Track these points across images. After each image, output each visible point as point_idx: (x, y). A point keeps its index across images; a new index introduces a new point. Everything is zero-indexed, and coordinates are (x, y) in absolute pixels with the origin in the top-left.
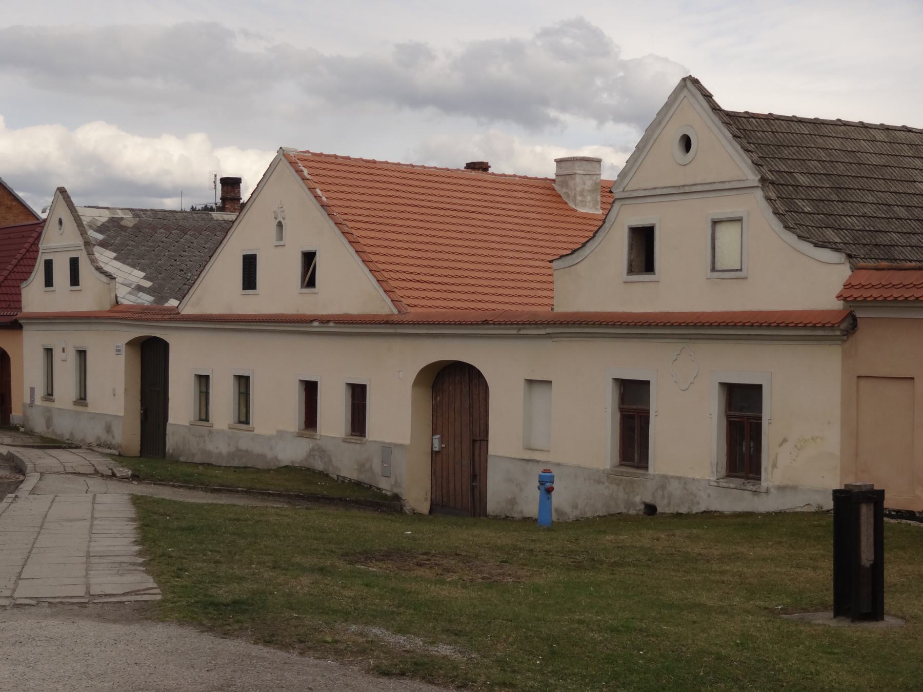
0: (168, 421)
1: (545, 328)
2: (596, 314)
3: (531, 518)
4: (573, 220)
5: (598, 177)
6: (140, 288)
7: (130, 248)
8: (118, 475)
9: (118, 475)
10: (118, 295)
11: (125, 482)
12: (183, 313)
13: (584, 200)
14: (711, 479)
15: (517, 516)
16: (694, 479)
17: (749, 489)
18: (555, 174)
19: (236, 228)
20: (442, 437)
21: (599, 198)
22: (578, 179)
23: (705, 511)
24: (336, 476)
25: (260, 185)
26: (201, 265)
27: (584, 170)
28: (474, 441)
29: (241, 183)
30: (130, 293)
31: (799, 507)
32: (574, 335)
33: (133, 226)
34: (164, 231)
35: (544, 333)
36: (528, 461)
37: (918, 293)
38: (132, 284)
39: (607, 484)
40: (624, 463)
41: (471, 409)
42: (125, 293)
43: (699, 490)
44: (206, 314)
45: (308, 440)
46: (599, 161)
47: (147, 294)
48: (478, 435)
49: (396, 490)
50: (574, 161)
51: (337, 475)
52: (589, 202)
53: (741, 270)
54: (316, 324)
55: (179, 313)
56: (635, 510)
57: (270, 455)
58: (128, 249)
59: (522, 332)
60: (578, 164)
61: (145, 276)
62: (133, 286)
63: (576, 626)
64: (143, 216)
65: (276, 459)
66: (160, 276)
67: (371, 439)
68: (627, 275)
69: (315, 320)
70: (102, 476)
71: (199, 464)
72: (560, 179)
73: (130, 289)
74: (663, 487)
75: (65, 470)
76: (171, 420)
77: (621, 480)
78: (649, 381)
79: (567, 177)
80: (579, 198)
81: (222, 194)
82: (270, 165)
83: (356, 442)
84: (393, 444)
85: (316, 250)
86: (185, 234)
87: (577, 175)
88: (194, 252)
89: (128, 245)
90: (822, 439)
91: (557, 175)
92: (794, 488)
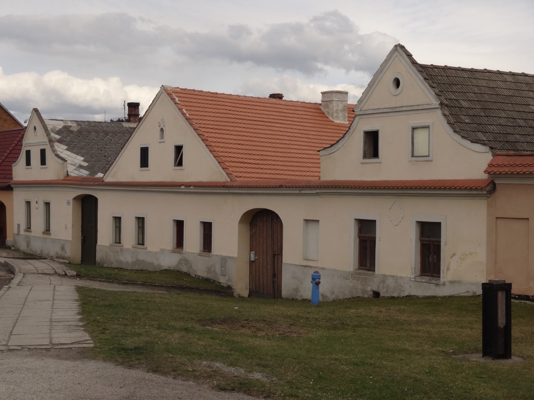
0: (97, 243)
1: (315, 190)
2: (345, 182)
3: (307, 299)
4: (332, 127)
5: (346, 102)
6: (81, 167)
7: (75, 143)
8: (68, 275)
9: (68, 275)
10: (68, 171)
11: (72, 279)
12: (106, 181)
13: (338, 115)
14: (412, 277)
15: (299, 298)
16: (401, 277)
17: (433, 283)
18: (321, 101)
19: (137, 132)
20: (256, 253)
21: (347, 115)
22: (334, 104)
23: (408, 296)
24: (194, 275)
25: (150, 107)
26: (116, 153)
27: (338, 99)
28: (274, 255)
29: (139, 106)
30: (75, 169)
31: (462, 293)
32: (332, 194)
33: (77, 130)
34: (95, 134)
35: (315, 193)
36: (306, 266)
37: (531, 170)
38: (77, 164)
39: (351, 280)
40: (361, 267)
41: (273, 236)
42: (73, 170)
43: (405, 283)
44: (119, 182)
45: (178, 254)
46: (346, 93)
47: (85, 170)
48: (277, 251)
49: (229, 283)
50: (332, 93)
51: (195, 275)
52: (341, 117)
53: (429, 156)
54: (183, 187)
55: (103, 181)
56: (368, 295)
57: (156, 263)
58: (74, 144)
59: (302, 192)
60: (334, 95)
61: (84, 160)
62: (77, 165)
63: (333, 362)
64: (83, 125)
65: (160, 265)
66: (93, 159)
67: (214, 254)
68: (363, 159)
69: (182, 185)
70: (59, 275)
71: (115, 268)
72: (324, 103)
73: (75, 167)
74: (383, 282)
75: (38, 272)
76: (99, 243)
77: (359, 277)
78: (376, 220)
79: (328, 102)
80: (335, 115)
81: (128, 112)
82: (156, 95)
83: (206, 255)
84: (228, 256)
85: (183, 145)
86: (107, 135)
87: (334, 101)
88: (112, 146)
89: (74, 141)
90: (476, 254)
91: (322, 101)
92: (459, 282)
